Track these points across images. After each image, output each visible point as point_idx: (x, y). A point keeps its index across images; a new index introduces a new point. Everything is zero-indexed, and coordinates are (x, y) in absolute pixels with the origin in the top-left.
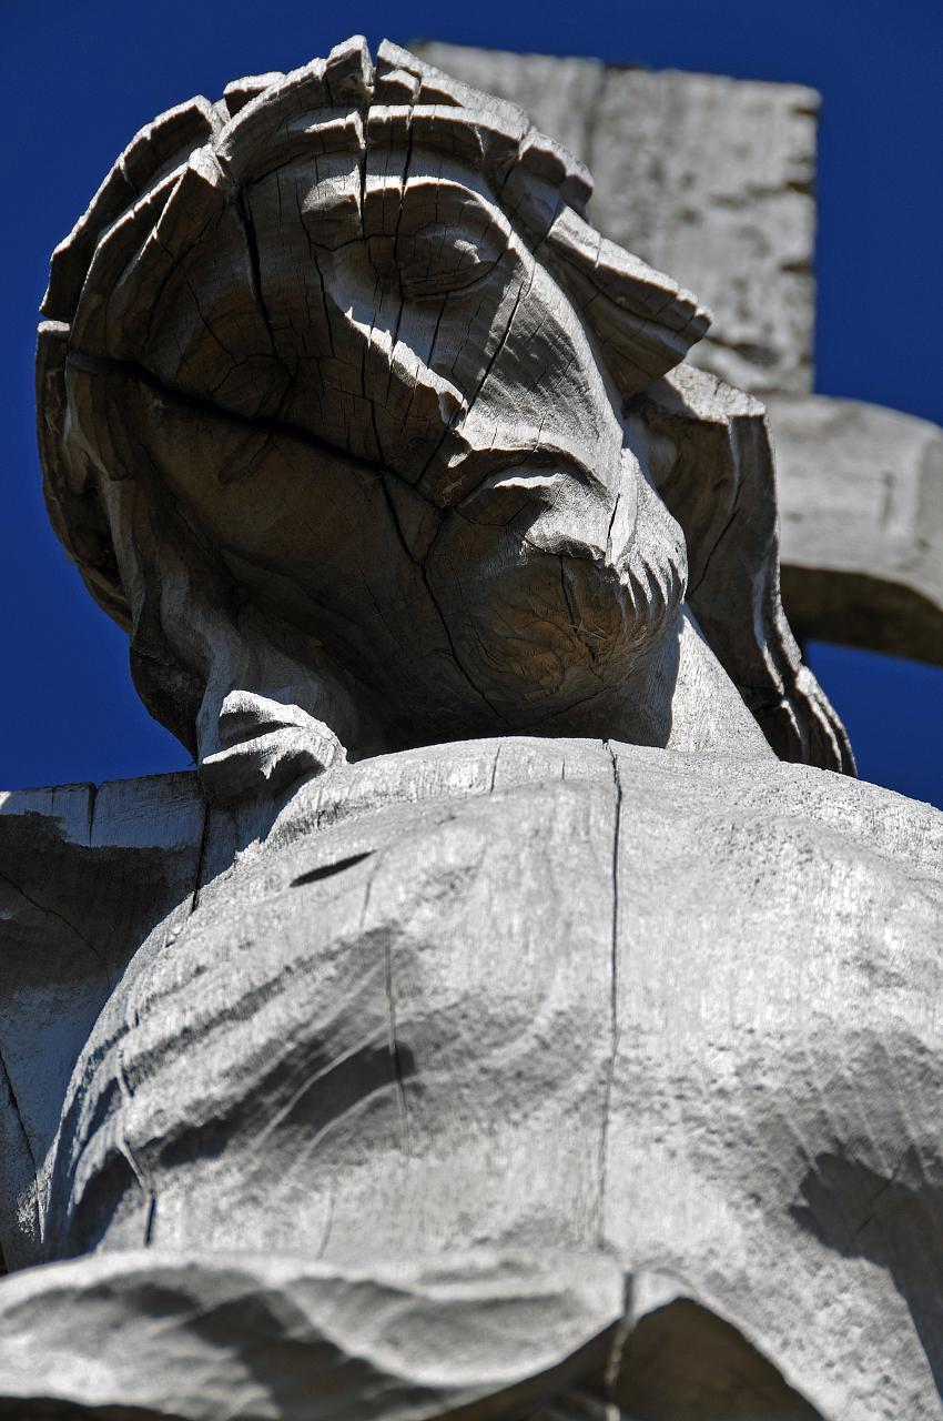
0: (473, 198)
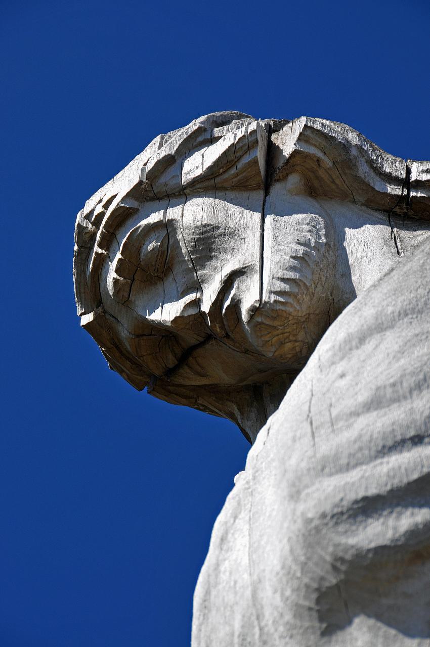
0: (139, 227)
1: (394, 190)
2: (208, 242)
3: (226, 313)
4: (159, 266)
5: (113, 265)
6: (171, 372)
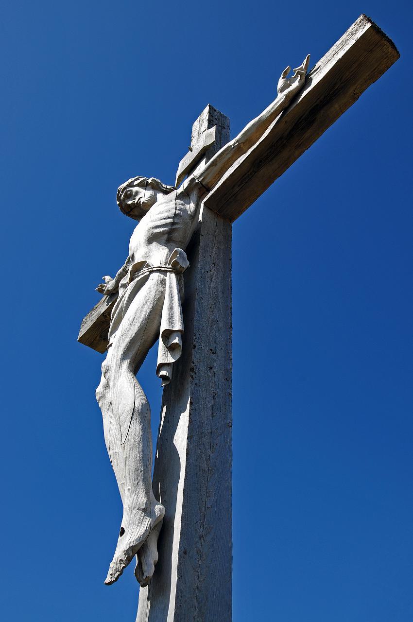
1: (164, 189)
2: (137, 193)
3: (139, 203)
4: (129, 196)
5: (123, 195)
6: (130, 212)
